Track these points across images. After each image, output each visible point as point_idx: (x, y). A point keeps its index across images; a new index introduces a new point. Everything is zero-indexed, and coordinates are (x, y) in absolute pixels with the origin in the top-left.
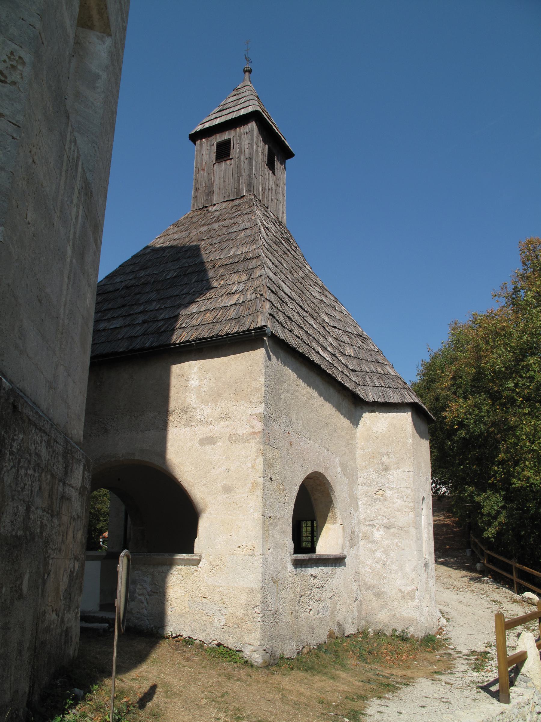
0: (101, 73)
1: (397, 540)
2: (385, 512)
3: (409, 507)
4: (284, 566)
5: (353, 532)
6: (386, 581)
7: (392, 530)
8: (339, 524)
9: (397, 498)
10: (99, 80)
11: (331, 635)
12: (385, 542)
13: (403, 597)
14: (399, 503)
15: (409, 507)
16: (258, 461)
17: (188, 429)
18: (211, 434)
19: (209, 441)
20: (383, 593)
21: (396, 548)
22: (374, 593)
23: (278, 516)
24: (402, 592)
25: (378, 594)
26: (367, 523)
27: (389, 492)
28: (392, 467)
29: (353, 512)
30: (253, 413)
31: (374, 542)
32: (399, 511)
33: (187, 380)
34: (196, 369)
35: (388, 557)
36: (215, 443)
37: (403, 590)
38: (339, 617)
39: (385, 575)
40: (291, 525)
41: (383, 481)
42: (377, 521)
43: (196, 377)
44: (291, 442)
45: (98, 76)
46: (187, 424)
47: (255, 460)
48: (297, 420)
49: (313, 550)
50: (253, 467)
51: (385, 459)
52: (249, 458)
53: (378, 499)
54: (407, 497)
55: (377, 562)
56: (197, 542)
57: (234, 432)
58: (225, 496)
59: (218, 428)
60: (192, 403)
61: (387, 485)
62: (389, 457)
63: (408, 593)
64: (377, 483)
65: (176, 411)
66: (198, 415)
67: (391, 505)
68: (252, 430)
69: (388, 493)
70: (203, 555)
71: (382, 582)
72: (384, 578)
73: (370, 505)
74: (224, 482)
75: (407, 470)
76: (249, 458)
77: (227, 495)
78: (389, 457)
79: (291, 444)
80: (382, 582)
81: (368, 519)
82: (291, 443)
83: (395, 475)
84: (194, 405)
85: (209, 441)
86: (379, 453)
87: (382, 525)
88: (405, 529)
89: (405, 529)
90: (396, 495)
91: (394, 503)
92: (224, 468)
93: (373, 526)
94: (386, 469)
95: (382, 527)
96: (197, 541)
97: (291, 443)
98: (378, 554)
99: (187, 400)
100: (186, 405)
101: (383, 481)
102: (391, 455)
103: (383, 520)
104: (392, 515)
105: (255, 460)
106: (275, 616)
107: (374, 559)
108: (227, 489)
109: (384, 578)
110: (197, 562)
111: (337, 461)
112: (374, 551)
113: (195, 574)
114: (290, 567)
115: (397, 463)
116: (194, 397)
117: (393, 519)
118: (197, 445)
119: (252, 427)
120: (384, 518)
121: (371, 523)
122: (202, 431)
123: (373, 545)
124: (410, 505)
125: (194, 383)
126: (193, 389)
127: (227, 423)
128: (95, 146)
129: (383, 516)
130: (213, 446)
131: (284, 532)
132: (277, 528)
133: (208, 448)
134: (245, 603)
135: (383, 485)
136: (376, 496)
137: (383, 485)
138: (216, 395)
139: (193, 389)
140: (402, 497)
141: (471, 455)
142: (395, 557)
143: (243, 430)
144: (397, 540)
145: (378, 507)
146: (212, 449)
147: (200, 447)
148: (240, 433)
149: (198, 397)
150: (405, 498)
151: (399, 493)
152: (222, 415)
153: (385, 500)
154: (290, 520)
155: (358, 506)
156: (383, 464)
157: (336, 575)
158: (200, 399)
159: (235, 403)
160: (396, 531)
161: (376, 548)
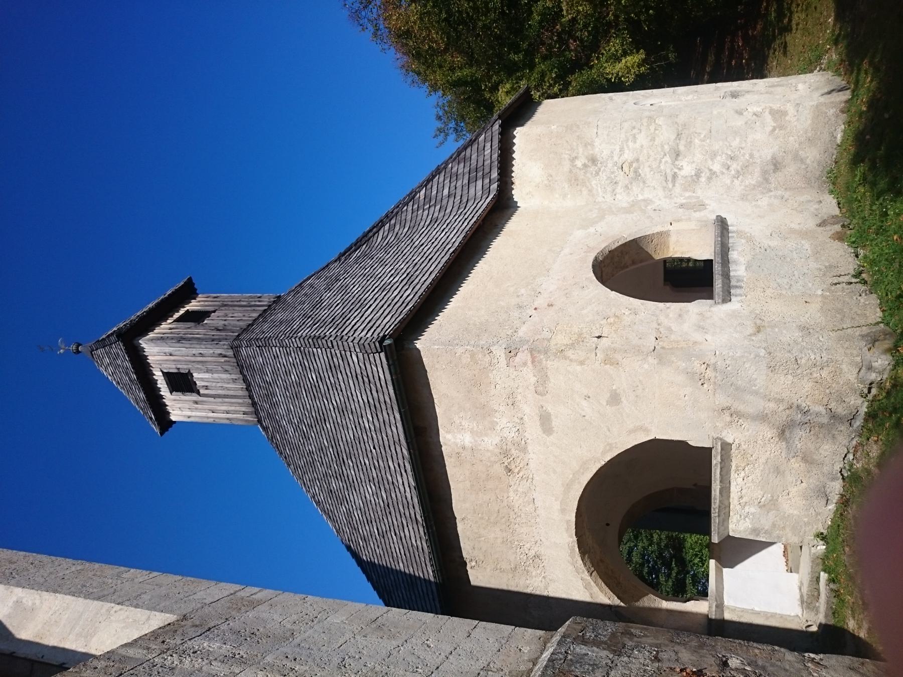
0: (15, 599)
1: (696, 141)
2: (655, 159)
3: (648, 126)
4: (734, 315)
5: (682, 206)
6: (756, 155)
7: (682, 148)
8: (671, 228)
9: (635, 142)
10: (24, 601)
11: (839, 237)
12: (698, 157)
13: (781, 127)
14: (642, 139)
15: (648, 126)
16: (572, 357)
17: (530, 448)
18: (537, 418)
19: (545, 421)
20: (774, 158)
21: (708, 141)
22: (774, 172)
23: (655, 325)
24: (774, 129)
25: (775, 165)
26: (670, 186)
27: (626, 156)
28: (591, 152)
29: (653, 207)
30: (505, 362)
31: (698, 175)
32: (653, 139)
33: (464, 448)
34: (449, 436)
35: (720, 153)
36: (549, 415)
37: (771, 128)
38: (811, 224)
39: (747, 157)
40: (668, 304)
41: (610, 165)
42: (668, 171)
43: (459, 436)
44: (549, 305)
45: (18, 602)
46: (524, 450)
47: (571, 360)
48: (518, 296)
49: (709, 263)
50: (582, 363)
51: (579, 163)
52: (569, 368)
53: (636, 172)
54: (634, 128)
55: (728, 168)
56: (695, 441)
57: (532, 388)
58: (625, 402)
59: (528, 410)
60: (494, 443)
61: (616, 159)
62: (576, 157)
63: (775, 120)
64: (613, 173)
65: (506, 464)
66: (511, 435)
67: (645, 151)
68: (529, 363)
69: (628, 156)
70: (715, 436)
71: (758, 161)
72: (751, 156)
73: (644, 182)
74: (605, 404)
75: (595, 131)
76: (569, 368)
77: (623, 399)
78: (576, 157)
79: (552, 305)
80: (758, 161)
81: (665, 184)
82: (551, 305)
83: (601, 149)
84: (497, 440)
85: (545, 421)
86: (571, 171)
87: (673, 164)
88: (680, 129)
89: (680, 129)
90: (630, 144)
91: (642, 146)
92: (584, 403)
93: (675, 176)
94: (593, 160)
95: (677, 163)
96: (691, 443)
97: (551, 305)
98: (716, 167)
99: (491, 448)
100: (497, 451)
101: (610, 165)
102: (574, 155)
103: (666, 162)
104: (660, 149)
105: (571, 360)
106: (811, 331)
107: (723, 173)
108: (615, 399)
109: (751, 156)
110: (726, 447)
111: (579, 234)
112: (713, 173)
113: (744, 447)
114: (734, 305)
115: (586, 146)
116: (486, 439)
117: (666, 147)
118: (551, 437)
119: (525, 364)
120: (663, 160)
121: (670, 178)
122: (533, 430)
123: (703, 175)
124: (645, 124)
125: (467, 439)
126: (476, 441)
127: (519, 397)
128: (114, 609)
129: (660, 162)
130: (553, 417)
131: (680, 315)
132: (673, 328)
133: (555, 423)
134: (790, 377)
135: (616, 164)
136: (632, 175)
137: (616, 164)
138: (483, 412)
139: (476, 441)
140: (634, 137)
141: (561, 25)
142: (721, 143)
143: (529, 376)
144: (696, 141)
145: (647, 170)
146: (557, 417)
147: (555, 434)
148: (533, 380)
149: (486, 435)
150: (635, 131)
151: (627, 140)
152: (510, 404)
153: (637, 160)
154: (661, 305)
155: (644, 200)
156: (585, 166)
157: (747, 230)
158: (489, 432)
159: (493, 387)
160: (683, 142)
161: (707, 171)
